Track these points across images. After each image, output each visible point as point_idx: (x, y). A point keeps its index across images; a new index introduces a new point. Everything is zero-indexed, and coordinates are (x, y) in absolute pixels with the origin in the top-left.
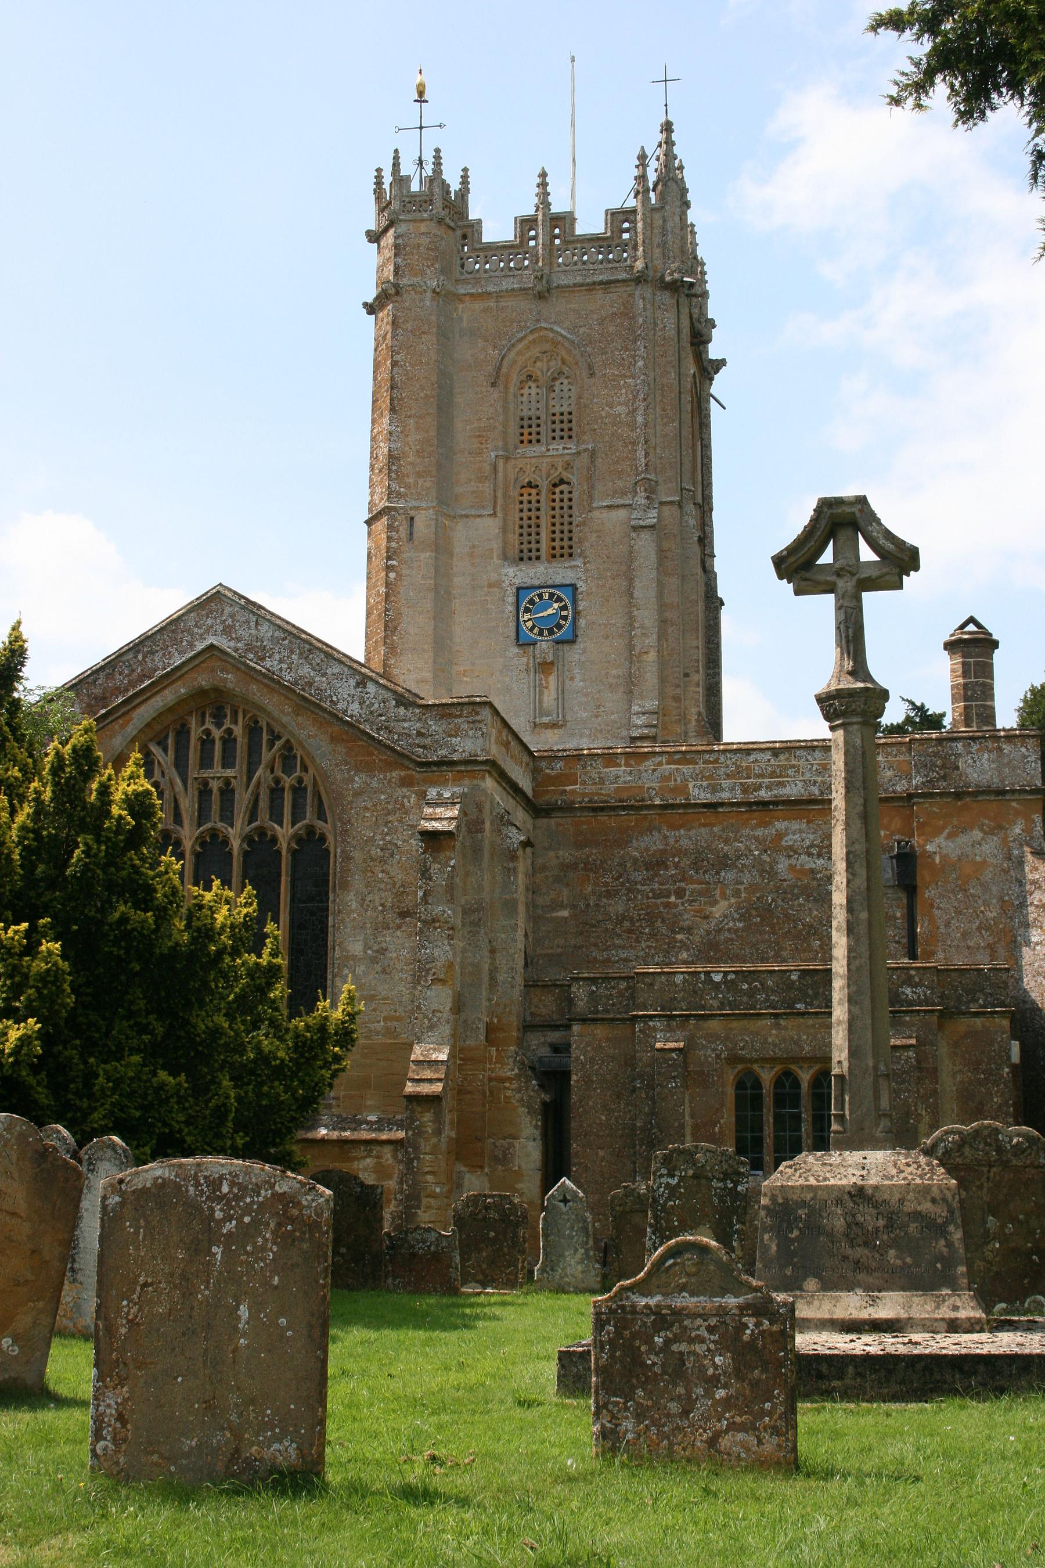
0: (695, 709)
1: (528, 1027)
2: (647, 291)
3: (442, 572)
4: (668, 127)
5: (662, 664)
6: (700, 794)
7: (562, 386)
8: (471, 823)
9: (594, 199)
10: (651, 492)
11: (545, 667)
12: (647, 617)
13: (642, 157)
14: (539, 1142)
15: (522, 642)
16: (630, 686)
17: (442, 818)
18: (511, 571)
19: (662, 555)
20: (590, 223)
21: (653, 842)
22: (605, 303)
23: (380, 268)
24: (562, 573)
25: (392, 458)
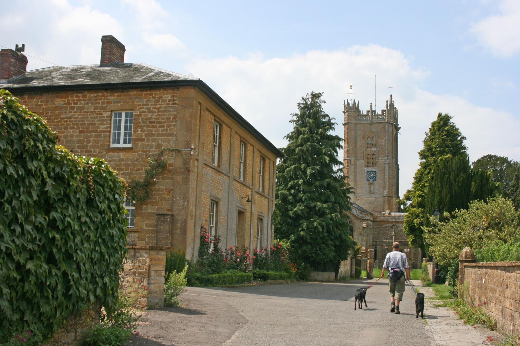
0: (394, 191)
1: (373, 245)
2: (387, 124)
3: (355, 169)
4: (391, 96)
5: (389, 184)
6: (391, 221)
7: (374, 138)
8: (367, 226)
9: (380, 107)
10: (388, 157)
11: (371, 184)
12: (387, 177)
13: (387, 101)
14: (86, 93)
15: (367, 180)
16: (384, 188)
17: (365, 225)
18: (366, 169)
19: (389, 167)
20: (379, 112)
21: (385, 225)
22: (381, 126)
23: (345, 118)
24: (374, 169)
25: (348, 151)
